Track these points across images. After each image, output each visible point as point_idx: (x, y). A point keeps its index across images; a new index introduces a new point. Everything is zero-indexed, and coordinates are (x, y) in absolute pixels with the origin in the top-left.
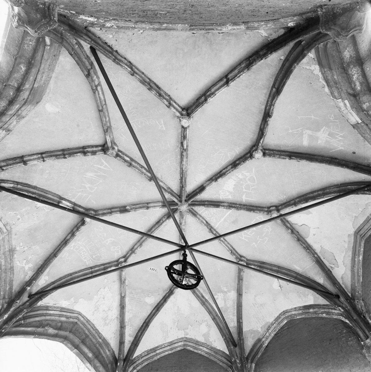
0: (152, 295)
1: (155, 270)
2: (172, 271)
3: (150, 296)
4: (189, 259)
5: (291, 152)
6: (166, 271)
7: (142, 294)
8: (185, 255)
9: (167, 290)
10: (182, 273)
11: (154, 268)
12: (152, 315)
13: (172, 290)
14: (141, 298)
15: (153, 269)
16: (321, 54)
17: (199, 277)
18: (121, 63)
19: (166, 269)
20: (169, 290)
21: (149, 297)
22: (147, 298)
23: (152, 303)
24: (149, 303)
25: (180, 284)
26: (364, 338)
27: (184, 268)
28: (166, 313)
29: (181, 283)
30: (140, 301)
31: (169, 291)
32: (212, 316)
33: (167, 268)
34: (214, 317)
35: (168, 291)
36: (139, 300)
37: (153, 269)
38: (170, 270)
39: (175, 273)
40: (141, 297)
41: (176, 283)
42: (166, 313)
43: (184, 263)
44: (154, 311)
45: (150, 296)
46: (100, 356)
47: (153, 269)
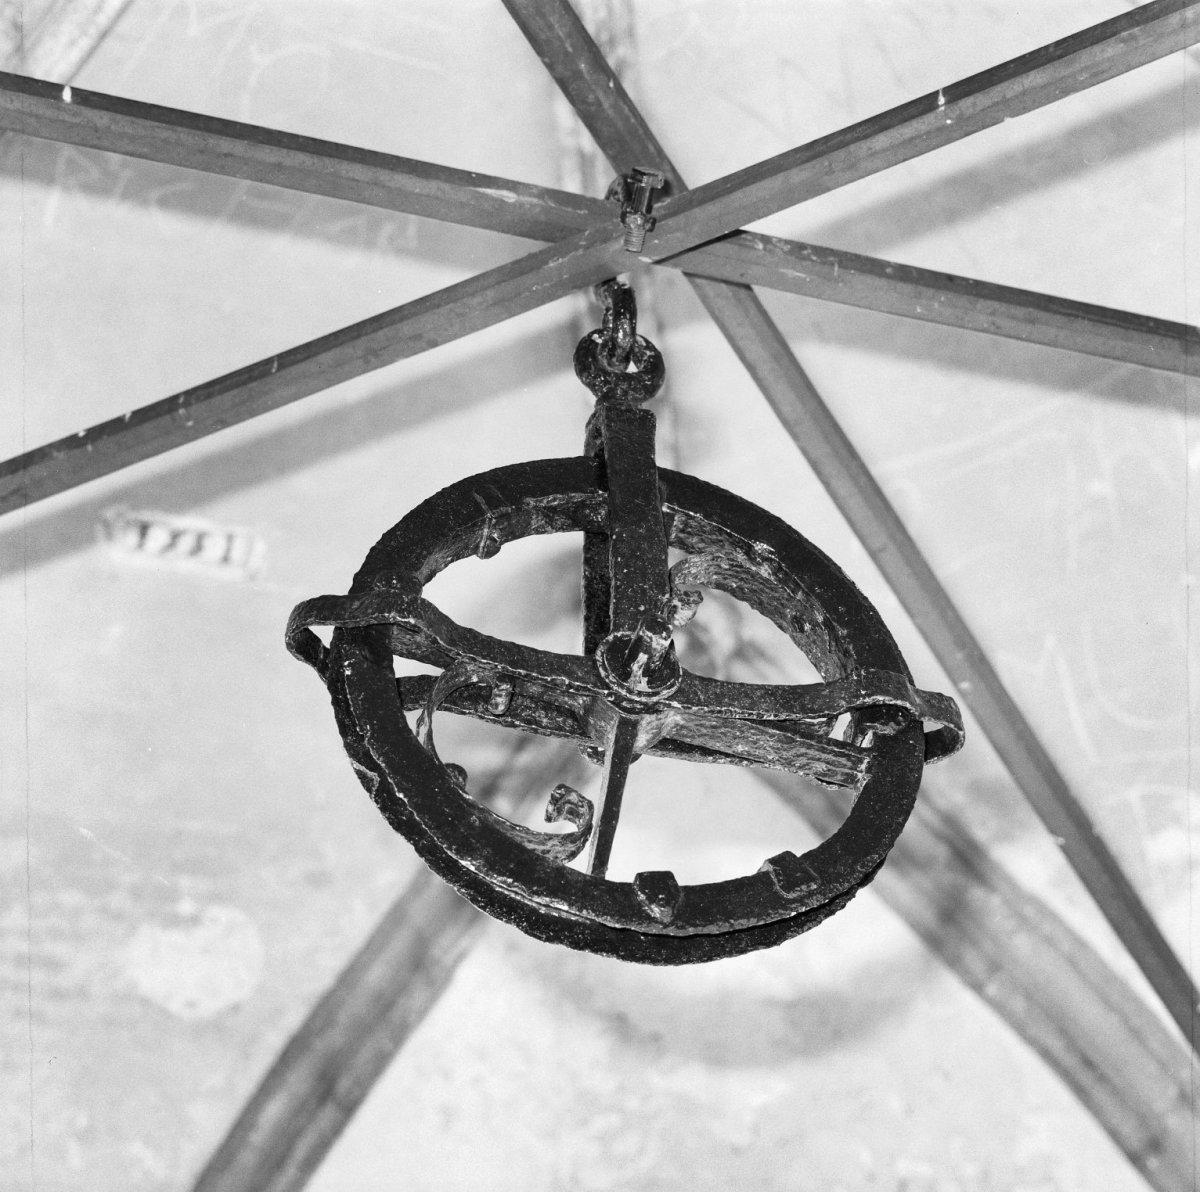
0: (216, 898)
2: (405, 667)
4: (725, 430)
6: (309, 672)
7: (70, 898)
8: (622, 376)
10: (606, 686)
12: (247, 1159)
14: (60, 950)
16: (759, 916)
17: (880, 749)
19: (303, 646)
21: (174, 921)
24: (191, 1005)
25: (561, 883)
27: (620, 596)
28: (448, 1115)
29: (582, 863)
30: (57, 994)
32: (1117, 1117)
33: (325, 633)
34: (1143, 1118)
36: (38, 977)
38: (365, 647)
39: (466, 698)
40: (56, 934)
41: (492, 867)
42: (448, 1115)
43: (622, 498)
44: (274, 1110)
46: (202, 125)
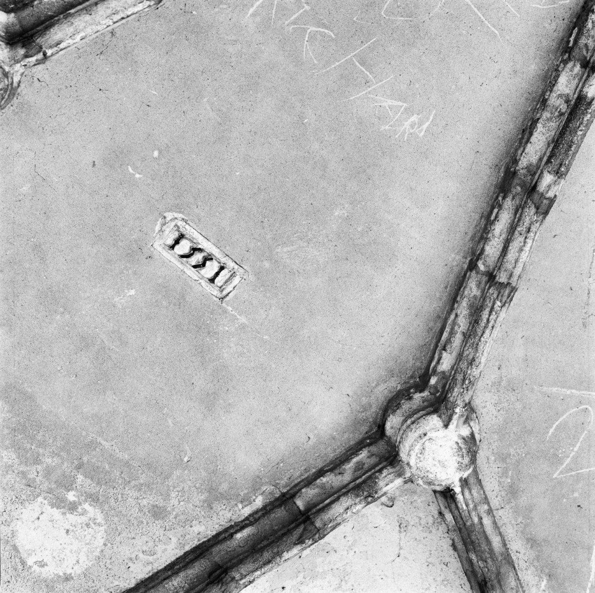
0: (94, 499)
1: (184, 247)
3: (71, 496)
5: (165, 567)
9: (246, 500)
11: (208, 247)
13: (300, 503)
15: (195, 250)
18: (526, 196)
20: (259, 502)
21: (59, 503)
22: (29, 512)
23: (68, 578)
24: (42, 564)
26: (459, 338)
31: (266, 510)
35: (247, 511)
37: (198, 258)
45: (71, 496)
47: (198, 258)
